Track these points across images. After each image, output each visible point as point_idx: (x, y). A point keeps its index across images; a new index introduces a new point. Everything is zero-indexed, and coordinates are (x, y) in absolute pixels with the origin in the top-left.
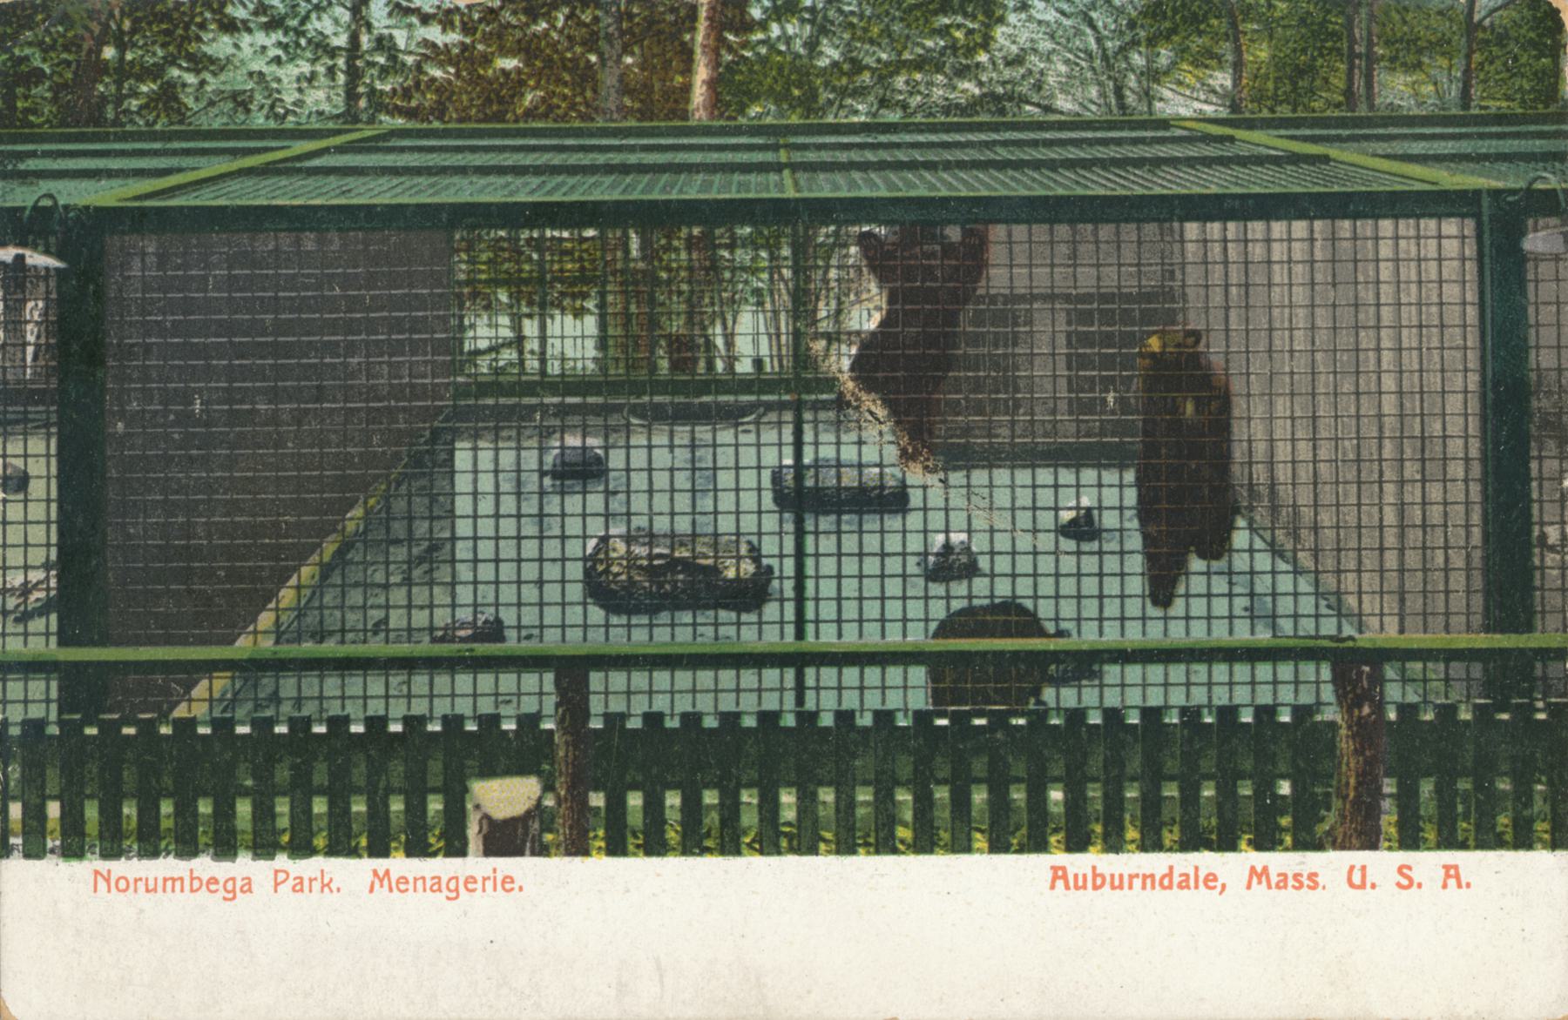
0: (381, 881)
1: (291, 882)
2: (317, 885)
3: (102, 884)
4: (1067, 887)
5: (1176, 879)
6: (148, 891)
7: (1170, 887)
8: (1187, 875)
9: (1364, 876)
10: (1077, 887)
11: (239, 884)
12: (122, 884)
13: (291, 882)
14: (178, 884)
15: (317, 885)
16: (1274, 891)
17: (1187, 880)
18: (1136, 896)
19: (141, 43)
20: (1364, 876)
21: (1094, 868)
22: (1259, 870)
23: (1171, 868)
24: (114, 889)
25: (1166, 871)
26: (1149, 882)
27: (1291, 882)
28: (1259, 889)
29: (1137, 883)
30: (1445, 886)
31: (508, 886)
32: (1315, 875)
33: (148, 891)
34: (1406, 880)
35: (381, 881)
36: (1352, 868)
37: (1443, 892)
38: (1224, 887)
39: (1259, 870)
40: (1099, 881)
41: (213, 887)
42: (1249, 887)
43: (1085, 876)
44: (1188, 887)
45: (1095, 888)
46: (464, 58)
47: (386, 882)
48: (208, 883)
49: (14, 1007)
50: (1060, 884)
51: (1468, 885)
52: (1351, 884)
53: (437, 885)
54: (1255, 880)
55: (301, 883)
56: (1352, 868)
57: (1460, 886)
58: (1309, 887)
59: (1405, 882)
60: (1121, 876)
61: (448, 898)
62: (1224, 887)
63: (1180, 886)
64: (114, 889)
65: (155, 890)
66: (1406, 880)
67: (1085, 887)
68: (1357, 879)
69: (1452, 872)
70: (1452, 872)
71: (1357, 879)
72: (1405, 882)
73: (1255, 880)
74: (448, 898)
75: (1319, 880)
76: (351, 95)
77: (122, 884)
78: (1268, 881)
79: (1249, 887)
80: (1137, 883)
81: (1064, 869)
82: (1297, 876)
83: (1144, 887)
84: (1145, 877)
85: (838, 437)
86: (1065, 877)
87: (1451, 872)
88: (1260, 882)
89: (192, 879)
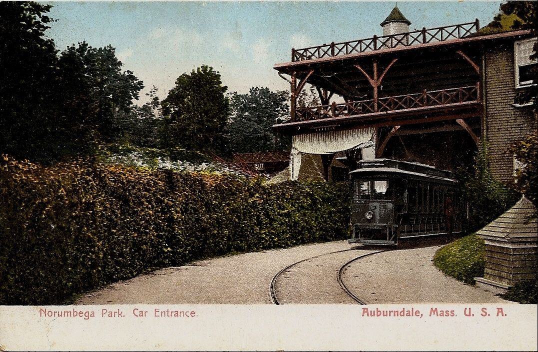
0: (434, 312)
1: (108, 313)
2: (117, 315)
3: (43, 314)
4: (368, 316)
5: (406, 313)
8: (409, 311)
9: (470, 312)
10: (372, 316)
12: (50, 314)
13: (108, 313)
14: (69, 313)
15: (117, 315)
17: (409, 313)
18: (392, 319)
19: (318, 213)
20: (470, 312)
24: (47, 315)
26: (396, 313)
27: (445, 314)
28: (434, 316)
29: (392, 314)
30: (498, 315)
31: (417, 314)
32: (453, 311)
34: (484, 313)
35: (434, 312)
36: (466, 309)
37: (430, 317)
38: (422, 315)
40: (379, 313)
41: (81, 315)
42: (430, 315)
43: (374, 311)
45: (378, 316)
47: (435, 313)
48: (79, 313)
50: (366, 314)
51: (506, 315)
52: (465, 314)
53: (396, 313)
54: (432, 313)
56: (466, 309)
59: (484, 314)
62: (422, 315)
64: (47, 315)
65: (61, 316)
66: (484, 313)
67: (374, 315)
68: (467, 313)
69: (500, 310)
71: (467, 313)
72: (484, 314)
73: (432, 313)
75: (455, 313)
76: (97, 176)
77: (50, 314)
79: (430, 315)
80: (392, 314)
82: (447, 312)
83: (394, 315)
86: (367, 312)
87: (500, 311)
89: (74, 312)
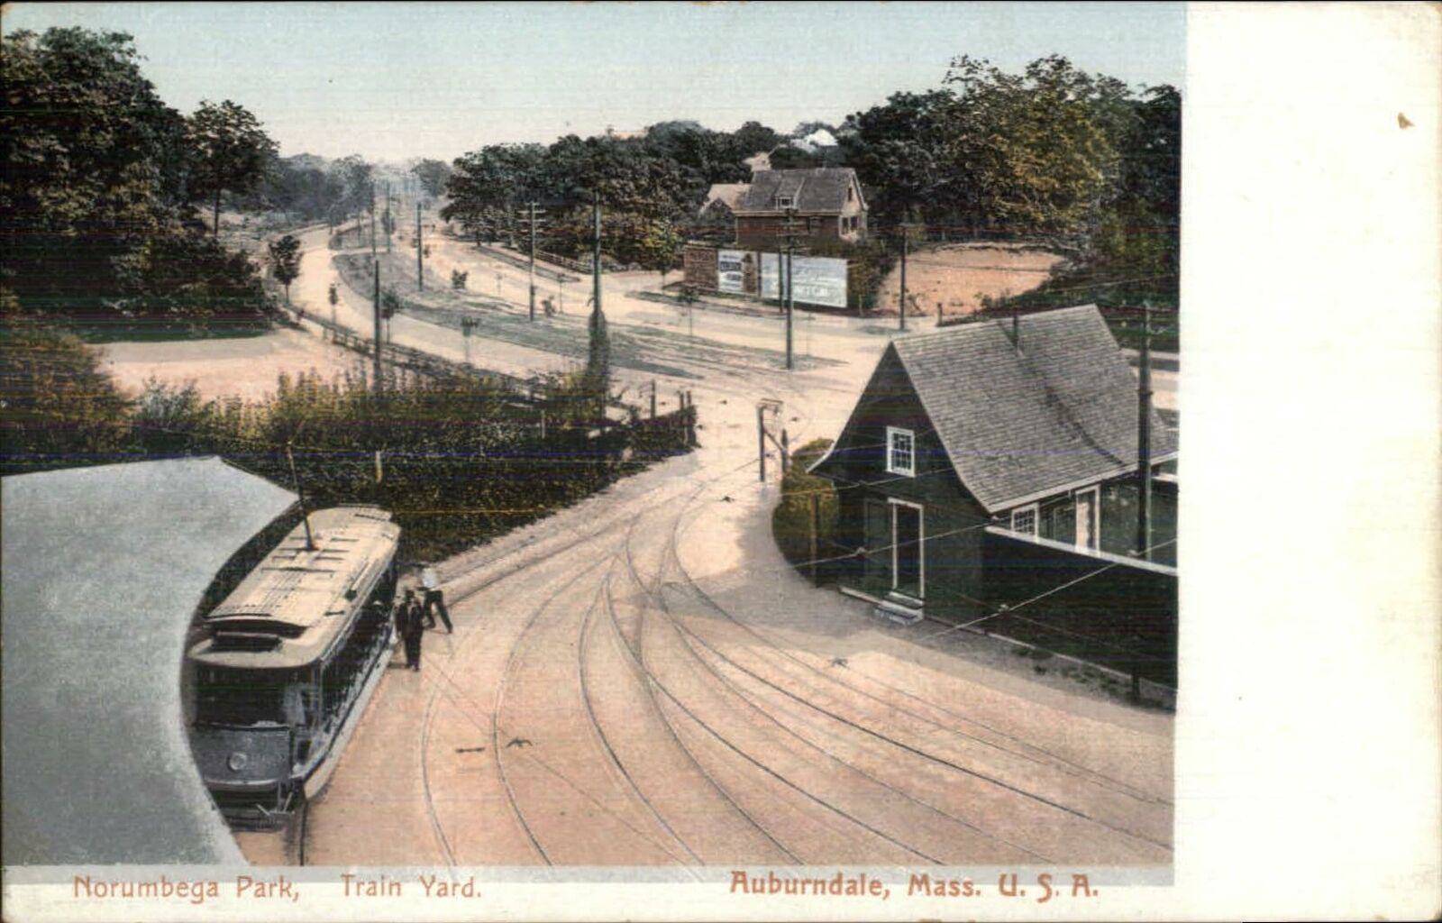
4: (746, 890)
6: (124, 895)
7: (839, 892)
11: (767, 886)
16: (933, 897)
21: (771, 874)
22: (919, 878)
23: (840, 875)
25: (835, 877)
27: (948, 888)
33: (124, 895)
38: (297, 895)
39: (919, 878)
44: (374, 894)
46: (879, 224)
49: (6, 917)
55: (446, 889)
57: (1087, 893)
58: (951, 894)
60: (140, 894)
61: (194, 902)
63: (848, 893)
70: (740, 878)
74: (194, 902)
78: (928, 890)
80: (809, 888)
81: (743, 874)
83: (815, 892)
84: (816, 882)
85: (1144, 355)
88: (920, 889)
